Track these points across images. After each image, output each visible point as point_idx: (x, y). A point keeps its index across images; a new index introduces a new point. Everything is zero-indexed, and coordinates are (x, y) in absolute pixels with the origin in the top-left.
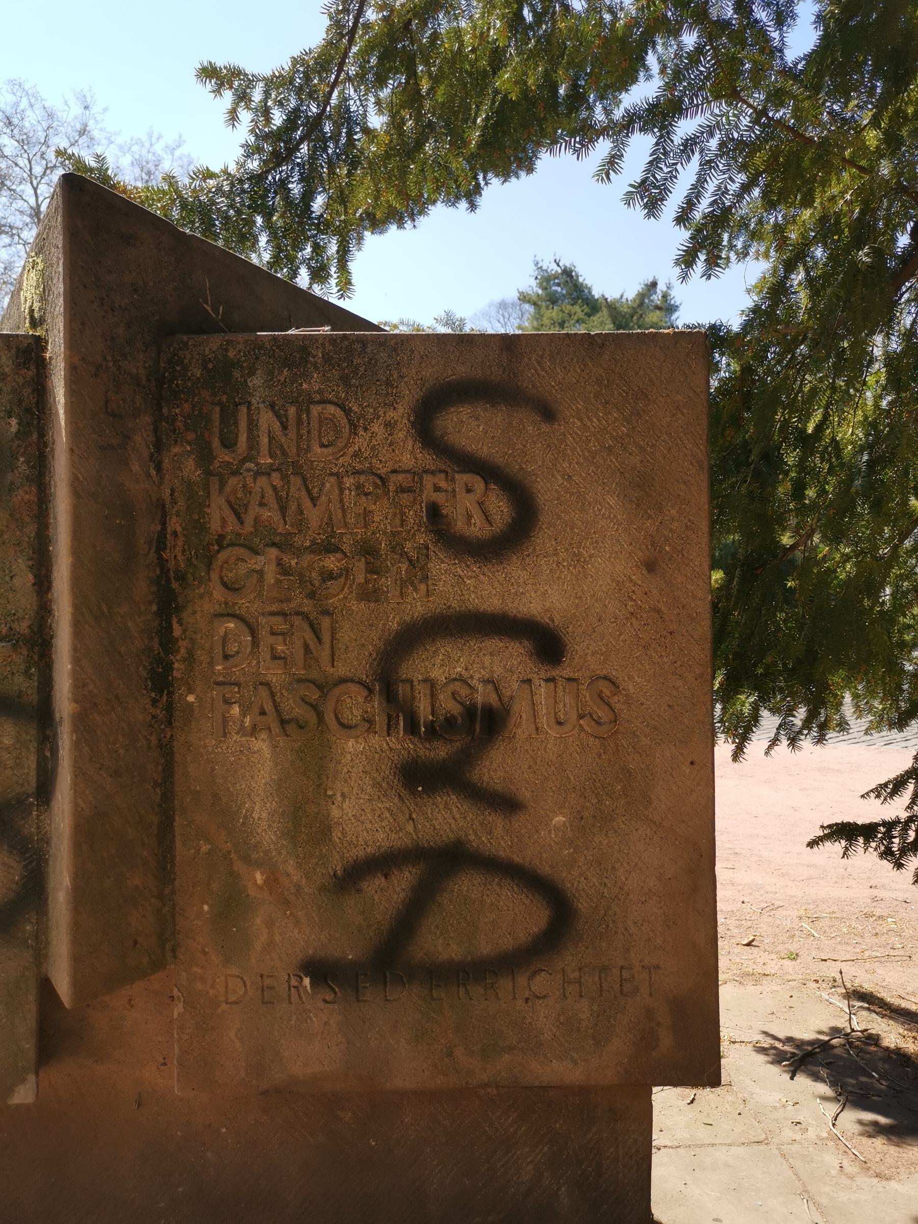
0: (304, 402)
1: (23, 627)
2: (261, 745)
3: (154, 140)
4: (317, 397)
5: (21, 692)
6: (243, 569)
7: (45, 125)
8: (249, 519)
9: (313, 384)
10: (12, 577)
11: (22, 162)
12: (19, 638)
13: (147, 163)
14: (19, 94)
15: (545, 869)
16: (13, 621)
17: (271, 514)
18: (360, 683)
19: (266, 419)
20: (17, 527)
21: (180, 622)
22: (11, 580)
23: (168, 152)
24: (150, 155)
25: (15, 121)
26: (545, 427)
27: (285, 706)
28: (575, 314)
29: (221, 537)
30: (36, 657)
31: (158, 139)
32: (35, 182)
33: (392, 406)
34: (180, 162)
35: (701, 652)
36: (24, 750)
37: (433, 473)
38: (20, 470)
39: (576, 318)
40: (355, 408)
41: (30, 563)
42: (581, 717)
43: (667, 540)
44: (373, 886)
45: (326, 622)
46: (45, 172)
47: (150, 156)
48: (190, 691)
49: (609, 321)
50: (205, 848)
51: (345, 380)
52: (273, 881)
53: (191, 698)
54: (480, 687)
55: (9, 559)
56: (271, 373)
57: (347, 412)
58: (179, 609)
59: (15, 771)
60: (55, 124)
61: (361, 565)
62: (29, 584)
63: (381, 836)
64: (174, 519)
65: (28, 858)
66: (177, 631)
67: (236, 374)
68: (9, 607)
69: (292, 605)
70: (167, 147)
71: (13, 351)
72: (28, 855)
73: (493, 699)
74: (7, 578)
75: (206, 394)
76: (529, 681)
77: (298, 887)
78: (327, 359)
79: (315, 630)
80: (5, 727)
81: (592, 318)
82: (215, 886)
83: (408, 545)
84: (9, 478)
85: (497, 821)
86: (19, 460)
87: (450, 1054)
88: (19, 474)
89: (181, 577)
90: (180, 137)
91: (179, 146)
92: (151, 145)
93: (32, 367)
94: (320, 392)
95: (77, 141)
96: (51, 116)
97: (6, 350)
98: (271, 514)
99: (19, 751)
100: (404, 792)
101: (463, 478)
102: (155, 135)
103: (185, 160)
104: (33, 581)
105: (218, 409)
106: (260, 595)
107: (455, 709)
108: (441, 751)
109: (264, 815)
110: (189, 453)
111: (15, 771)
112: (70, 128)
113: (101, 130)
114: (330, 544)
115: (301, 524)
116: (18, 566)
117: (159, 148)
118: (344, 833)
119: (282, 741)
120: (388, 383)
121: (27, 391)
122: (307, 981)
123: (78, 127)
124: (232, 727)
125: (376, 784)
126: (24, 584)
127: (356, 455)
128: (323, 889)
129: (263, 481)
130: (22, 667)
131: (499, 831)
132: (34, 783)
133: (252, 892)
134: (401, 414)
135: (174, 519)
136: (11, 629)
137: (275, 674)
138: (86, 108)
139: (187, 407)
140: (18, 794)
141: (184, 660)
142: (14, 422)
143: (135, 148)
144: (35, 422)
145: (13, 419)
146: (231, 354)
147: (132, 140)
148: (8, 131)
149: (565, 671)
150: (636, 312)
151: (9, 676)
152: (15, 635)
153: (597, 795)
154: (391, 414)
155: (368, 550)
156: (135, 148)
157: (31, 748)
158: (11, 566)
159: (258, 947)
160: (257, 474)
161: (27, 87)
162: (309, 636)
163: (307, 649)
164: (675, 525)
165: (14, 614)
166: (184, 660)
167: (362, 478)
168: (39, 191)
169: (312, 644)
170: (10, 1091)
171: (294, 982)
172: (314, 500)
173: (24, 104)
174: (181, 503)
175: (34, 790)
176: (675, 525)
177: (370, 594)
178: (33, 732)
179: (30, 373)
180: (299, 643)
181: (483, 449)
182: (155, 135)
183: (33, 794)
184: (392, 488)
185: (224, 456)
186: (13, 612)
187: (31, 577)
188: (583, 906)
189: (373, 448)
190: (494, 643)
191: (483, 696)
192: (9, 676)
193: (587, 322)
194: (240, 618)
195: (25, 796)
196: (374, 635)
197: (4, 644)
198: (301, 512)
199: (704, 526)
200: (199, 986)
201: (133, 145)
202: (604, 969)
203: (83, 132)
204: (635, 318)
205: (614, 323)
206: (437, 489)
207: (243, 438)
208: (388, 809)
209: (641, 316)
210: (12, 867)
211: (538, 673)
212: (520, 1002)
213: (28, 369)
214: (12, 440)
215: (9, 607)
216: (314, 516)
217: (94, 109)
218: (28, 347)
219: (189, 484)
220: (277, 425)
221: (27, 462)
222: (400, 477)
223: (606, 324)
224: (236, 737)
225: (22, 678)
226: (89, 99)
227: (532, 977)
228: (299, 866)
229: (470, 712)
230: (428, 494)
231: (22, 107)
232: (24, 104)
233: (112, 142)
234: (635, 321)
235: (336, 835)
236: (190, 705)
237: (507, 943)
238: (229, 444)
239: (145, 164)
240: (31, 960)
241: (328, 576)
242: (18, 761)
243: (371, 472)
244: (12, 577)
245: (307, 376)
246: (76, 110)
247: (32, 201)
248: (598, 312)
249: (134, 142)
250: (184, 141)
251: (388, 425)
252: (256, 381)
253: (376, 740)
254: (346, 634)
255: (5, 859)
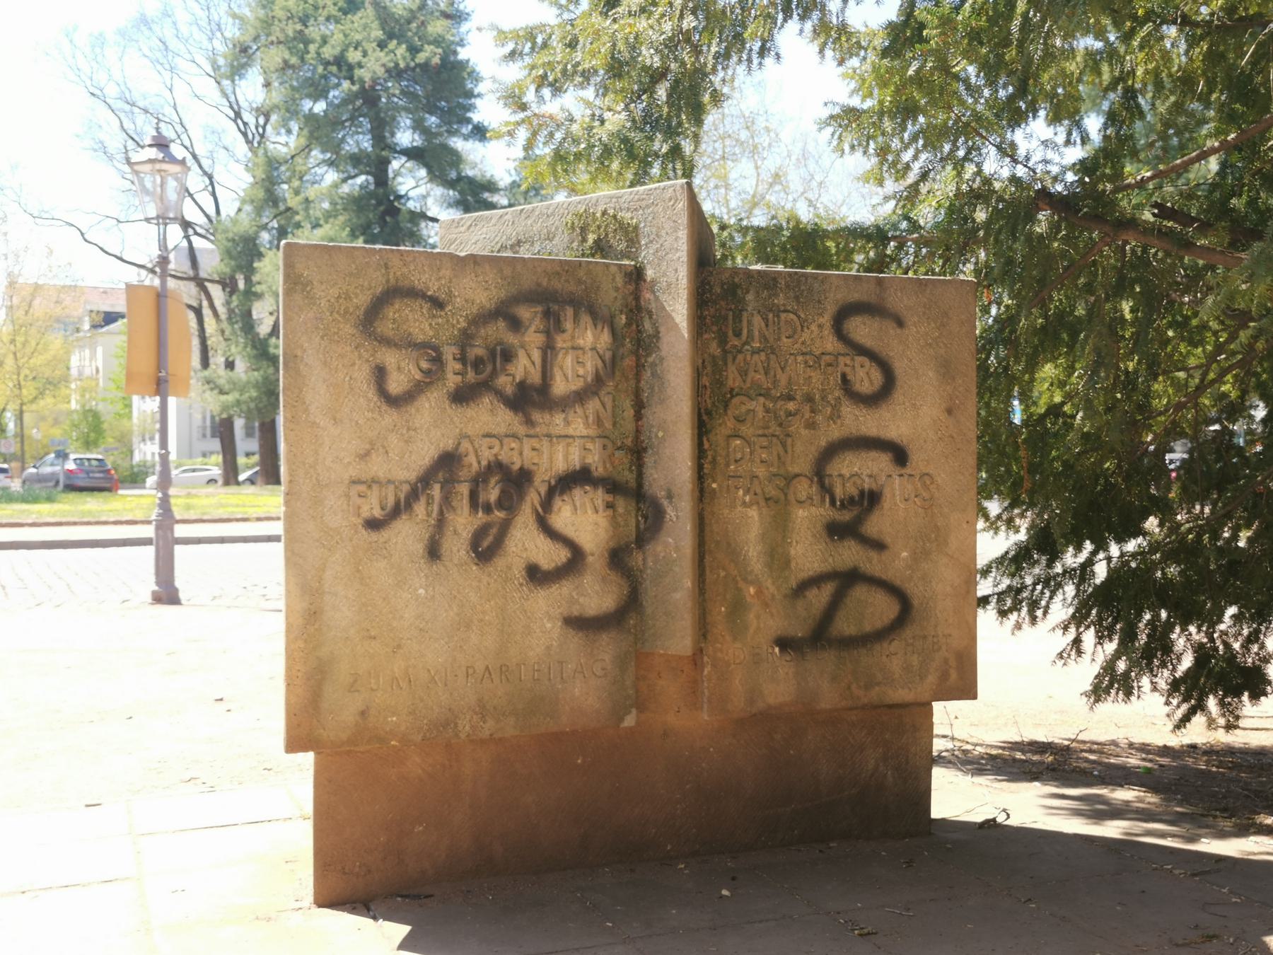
0: (778, 312)
2: (753, 513)
4: (782, 308)
6: (744, 409)
8: (749, 380)
9: (780, 300)
15: (898, 582)
17: (760, 377)
18: (806, 476)
19: (757, 321)
21: (708, 440)
26: (899, 331)
27: (766, 490)
28: (324, 7)
29: (732, 389)
33: (821, 315)
35: (972, 461)
37: (843, 355)
39: (325, 13)
40: (802, 316)
42: (916, 496)
43: (957, 397)
44: (812, 594)
45: (789, 440)
48: (714, 481)
49: (376, 25)
50: (723, 574)
51: (797, 298)
52: (759, 592)
53: (714, 486)
54: (867, 479)
56: (758, 293)
57: (799, 317)
58: (707, 433)
61: (807, 408)
63: (816, 565)
64: (705, 378)
66: (706, 446)
67: (739, 292)
69: (770, 431)
73: (874, 487)
75: (723, 303)
76: (890, 476)
77: (773, 596)
78: (788, 286)
79: (784, 445)
81: (349, 16)
82: (728, 596)
83: (830, 396)
85: (873, 554)
87: (849, 688)
89: (709, 413)
94: (784, 305)
98: (760, 377)
100: (828, 540)
101: (859, 359)
105: (731, 313)
106: (753, 424)
107: (855, 492)
108: (846, 516)
109: (755, 554)
110: (714, 338)
114: (790, 395)
115: (775, 382)
118: (797, 564)
119: (765, 511)
120: (819, 302)
121: (630, 299)
122: (777, 650)
124: (739, 503)
125: (814, 536)
127: (803, 343)
128: (785, 596)
129: (756, 357)
131: (875, 561)
132: (634, 536)
133: (749, 599)
134: (826, 320)
135: (705, 378)
137: (761, 471)
139: (712, 310)
141: (710, 463)
146: (736, 280)
149: (908, 471)
150: (415, 17)
153: (923, 541)
154: (821, 320)
155: (809, 399)
159: (751, 631)
160: (753, 353)
162: (780, 449)
163: (779, 458)
164: (961, 389)
166: (710, 463)
167: (808, 357)
169: (782, 453)
171: (770, 651)
172: (783, 369)
174: (709, 369)
176: (961, 389)
177: (811, 425)
178: (634, 505)
180: (775, 453)
181: (868, 342)
184: (823, 363)
185: (736, 342)
188: (915, 602)
189: (812, 340)
190: (874, 454)
191: (867, 485)
193: (342, 22)
194: (744, 438)
196: (813, 449)
198: (775, 376)
199: (975, 391)
200: (719, 655)
202: (925, 637)
204: (414, 25)
205: (383, 29)
206: (846, 365)
207: (745, 331)
208: (820, 550)
209: (423, 23)
211: (895, 471)
212: (884, 657)
216: (783, 379)
219: (714, 357)
220: (763, 324)
222: (828, 357)
223: (371, 28)
224: (740, 508)
227: (890, 643)
228: (773, 583)
229: (862, 493)
230: (841, 368)
234: (414, 30)
235: (793, 565)
236: (714, 490)
237: (879, 625)
238: (738, 334)
241: (789, 414)
243: (810, 353)
245: (776, 295)
248: (358, 9)
251: (820, 326)
252: (750, 297)
253: (813, 509)
254: (799, 448)
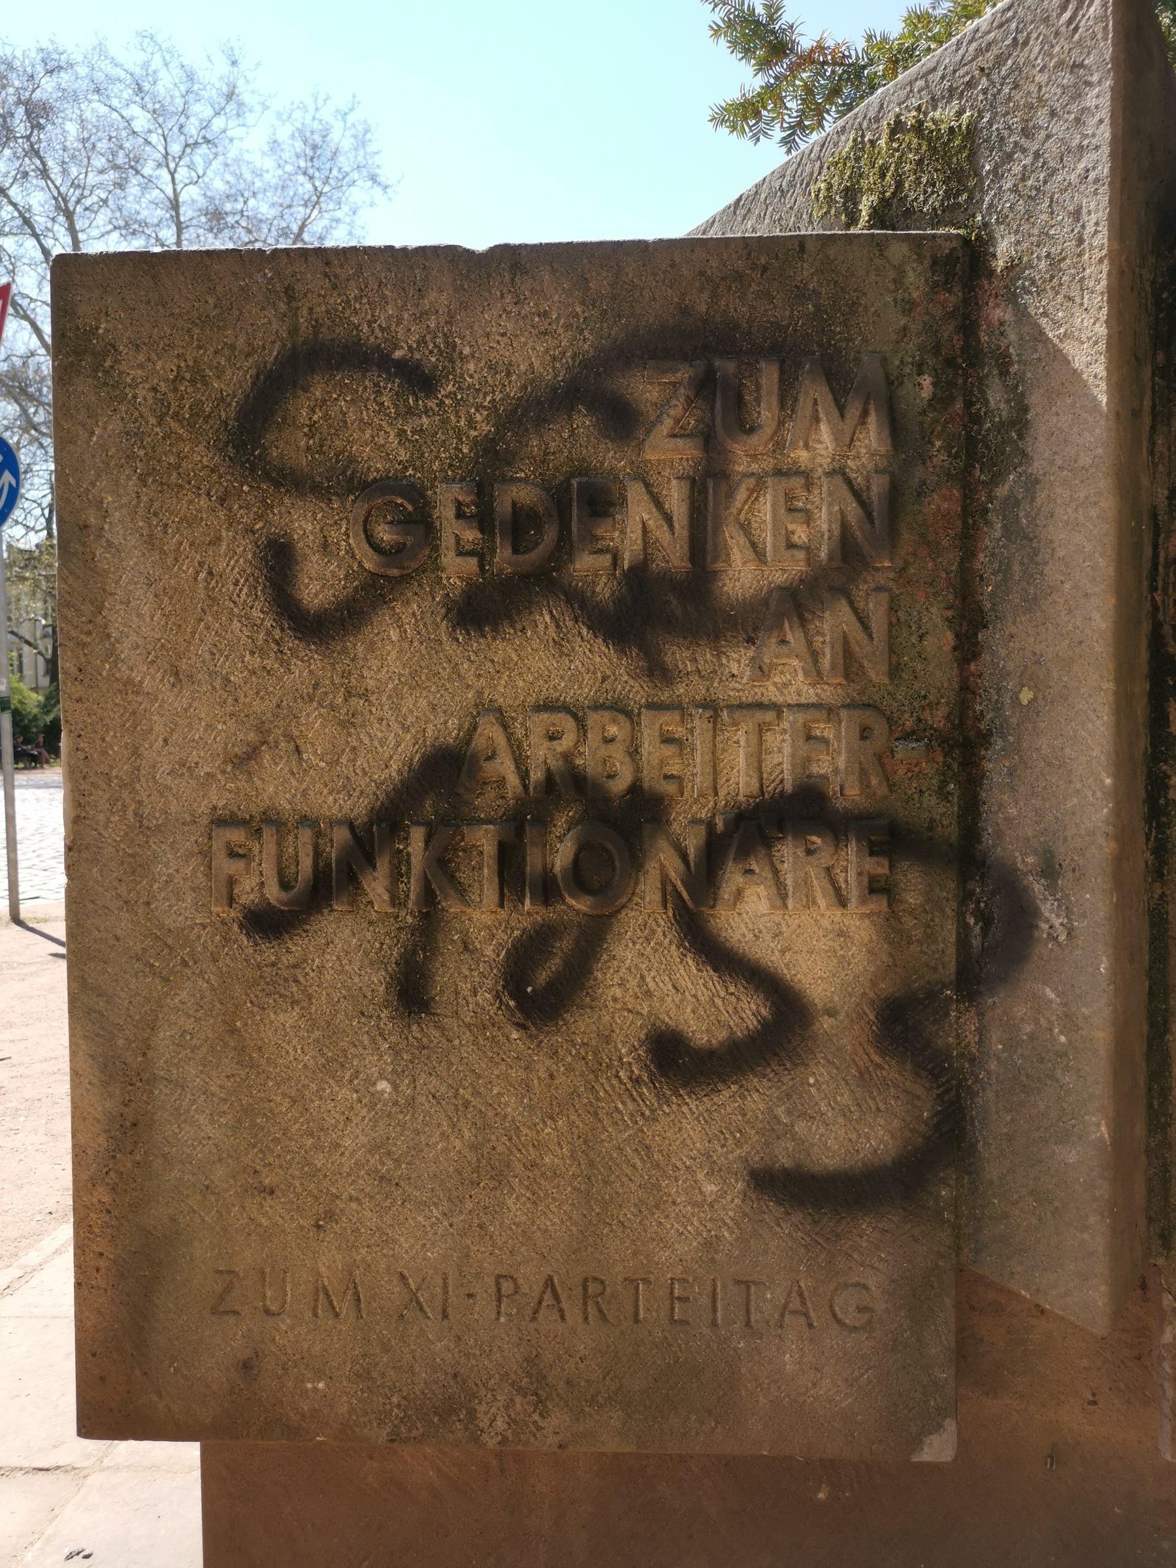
1: (938, 718)
3: (320, 103)
5: (932, 821)
7: (183, 88)
10: (921, 637)
11: (154, 138)
12: (932, 735)
13: (312, 133)
14: (150, 50)
16: (923, 708)
20: (930, 555)
22: (920, 641)
23: (339, 117)
24: (316, 122)
25: (146, 86)
30: (955, 766)
31: (325, 101)
32: (172, 165)
34: (353, 131)
36: (937, 914)
38: (935, 460)
41: (950, 613)
46: (184, 151)
47: (316, 125)
55: (918, 607)
59: (924, 947)
60: (196, 87)
62: (947, 648)
65: (943, 1084)
68: (916, 686)
70: (337, 111)
71: (927, 263)
72: (943, 1080)
74: (914, 639)
80: (909, 877)
84: (918, 474)
86: (933, 446)
88: (934, 467)
90: (354, 97)
91: (351, 110)
92: (317, 109)
93: (956, 289)
95: (223, 109)
96: (190, 77)
97: (915, 261)
99: (930, 916)
102: (321, 97)
103: (360, 128)
104: (952, 643)
111: (924, 947)
112: (214, 91)
113: (253, 92)
116: (931, 619)
117: (326, 114)
121: (948, 330)
123: (225, 89)
126: (940, 648)
130: (934, 781)
132: (952, 967)
136: (920, 720)
138: (234, 63)
140: (929, 982)
142: (927, 381)
143: (297, 115)
144: (960, 381)
145: (926, 377)
147: (292, 104)
148: (138, 99)
151: (916, 796)
152: (925, 730)
156: (297, 115)
157: (948, 911)
158: (920, 619)
161: (159, 40)
165: (925, 697)
168: (176, 176)
170: (916, 1443)
173: (157, 63)
175: (953, 977)
179: (953, 299)
182: (321, 97)
183: (950, 983)
186: (923, 693)
187: (950, 636)
192: (916, 796)
195: (940, 986)
197: (914, 745)
201: (293, 110)
203: (230, 96)
210: (918, 1098)
213: (950, 291)
214: (924, 413)
215: (916, 686)
217: (243, 65)
218: (951, 253)
221: (948, 448)
225: (934, 800)
226: (237, 52)
231: (153, 67)
232: (157, 63)
233: (268, 108)
239: (308, 134)
240: (948, 1243)
242: (929, 931)
244: (921, 637)
246: (222, 67)
247: (170, 192)
249: (295, 106)
250: (359, 103)
255: (908, 1083)
